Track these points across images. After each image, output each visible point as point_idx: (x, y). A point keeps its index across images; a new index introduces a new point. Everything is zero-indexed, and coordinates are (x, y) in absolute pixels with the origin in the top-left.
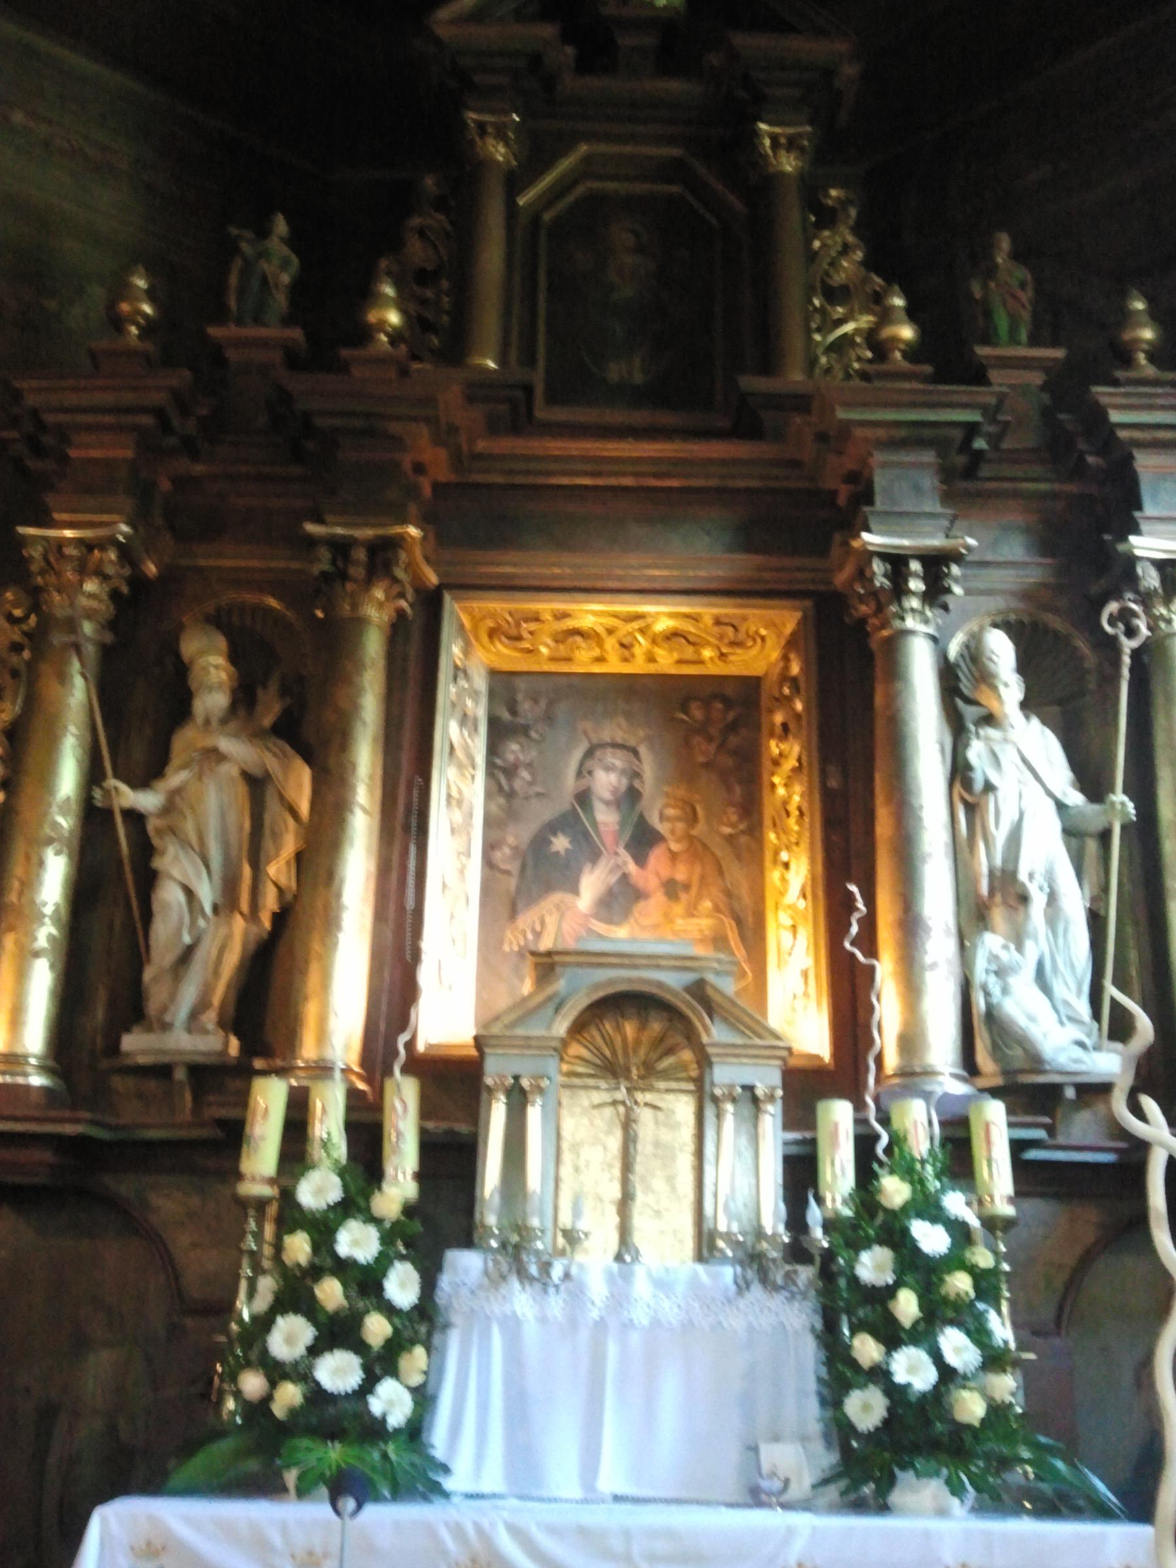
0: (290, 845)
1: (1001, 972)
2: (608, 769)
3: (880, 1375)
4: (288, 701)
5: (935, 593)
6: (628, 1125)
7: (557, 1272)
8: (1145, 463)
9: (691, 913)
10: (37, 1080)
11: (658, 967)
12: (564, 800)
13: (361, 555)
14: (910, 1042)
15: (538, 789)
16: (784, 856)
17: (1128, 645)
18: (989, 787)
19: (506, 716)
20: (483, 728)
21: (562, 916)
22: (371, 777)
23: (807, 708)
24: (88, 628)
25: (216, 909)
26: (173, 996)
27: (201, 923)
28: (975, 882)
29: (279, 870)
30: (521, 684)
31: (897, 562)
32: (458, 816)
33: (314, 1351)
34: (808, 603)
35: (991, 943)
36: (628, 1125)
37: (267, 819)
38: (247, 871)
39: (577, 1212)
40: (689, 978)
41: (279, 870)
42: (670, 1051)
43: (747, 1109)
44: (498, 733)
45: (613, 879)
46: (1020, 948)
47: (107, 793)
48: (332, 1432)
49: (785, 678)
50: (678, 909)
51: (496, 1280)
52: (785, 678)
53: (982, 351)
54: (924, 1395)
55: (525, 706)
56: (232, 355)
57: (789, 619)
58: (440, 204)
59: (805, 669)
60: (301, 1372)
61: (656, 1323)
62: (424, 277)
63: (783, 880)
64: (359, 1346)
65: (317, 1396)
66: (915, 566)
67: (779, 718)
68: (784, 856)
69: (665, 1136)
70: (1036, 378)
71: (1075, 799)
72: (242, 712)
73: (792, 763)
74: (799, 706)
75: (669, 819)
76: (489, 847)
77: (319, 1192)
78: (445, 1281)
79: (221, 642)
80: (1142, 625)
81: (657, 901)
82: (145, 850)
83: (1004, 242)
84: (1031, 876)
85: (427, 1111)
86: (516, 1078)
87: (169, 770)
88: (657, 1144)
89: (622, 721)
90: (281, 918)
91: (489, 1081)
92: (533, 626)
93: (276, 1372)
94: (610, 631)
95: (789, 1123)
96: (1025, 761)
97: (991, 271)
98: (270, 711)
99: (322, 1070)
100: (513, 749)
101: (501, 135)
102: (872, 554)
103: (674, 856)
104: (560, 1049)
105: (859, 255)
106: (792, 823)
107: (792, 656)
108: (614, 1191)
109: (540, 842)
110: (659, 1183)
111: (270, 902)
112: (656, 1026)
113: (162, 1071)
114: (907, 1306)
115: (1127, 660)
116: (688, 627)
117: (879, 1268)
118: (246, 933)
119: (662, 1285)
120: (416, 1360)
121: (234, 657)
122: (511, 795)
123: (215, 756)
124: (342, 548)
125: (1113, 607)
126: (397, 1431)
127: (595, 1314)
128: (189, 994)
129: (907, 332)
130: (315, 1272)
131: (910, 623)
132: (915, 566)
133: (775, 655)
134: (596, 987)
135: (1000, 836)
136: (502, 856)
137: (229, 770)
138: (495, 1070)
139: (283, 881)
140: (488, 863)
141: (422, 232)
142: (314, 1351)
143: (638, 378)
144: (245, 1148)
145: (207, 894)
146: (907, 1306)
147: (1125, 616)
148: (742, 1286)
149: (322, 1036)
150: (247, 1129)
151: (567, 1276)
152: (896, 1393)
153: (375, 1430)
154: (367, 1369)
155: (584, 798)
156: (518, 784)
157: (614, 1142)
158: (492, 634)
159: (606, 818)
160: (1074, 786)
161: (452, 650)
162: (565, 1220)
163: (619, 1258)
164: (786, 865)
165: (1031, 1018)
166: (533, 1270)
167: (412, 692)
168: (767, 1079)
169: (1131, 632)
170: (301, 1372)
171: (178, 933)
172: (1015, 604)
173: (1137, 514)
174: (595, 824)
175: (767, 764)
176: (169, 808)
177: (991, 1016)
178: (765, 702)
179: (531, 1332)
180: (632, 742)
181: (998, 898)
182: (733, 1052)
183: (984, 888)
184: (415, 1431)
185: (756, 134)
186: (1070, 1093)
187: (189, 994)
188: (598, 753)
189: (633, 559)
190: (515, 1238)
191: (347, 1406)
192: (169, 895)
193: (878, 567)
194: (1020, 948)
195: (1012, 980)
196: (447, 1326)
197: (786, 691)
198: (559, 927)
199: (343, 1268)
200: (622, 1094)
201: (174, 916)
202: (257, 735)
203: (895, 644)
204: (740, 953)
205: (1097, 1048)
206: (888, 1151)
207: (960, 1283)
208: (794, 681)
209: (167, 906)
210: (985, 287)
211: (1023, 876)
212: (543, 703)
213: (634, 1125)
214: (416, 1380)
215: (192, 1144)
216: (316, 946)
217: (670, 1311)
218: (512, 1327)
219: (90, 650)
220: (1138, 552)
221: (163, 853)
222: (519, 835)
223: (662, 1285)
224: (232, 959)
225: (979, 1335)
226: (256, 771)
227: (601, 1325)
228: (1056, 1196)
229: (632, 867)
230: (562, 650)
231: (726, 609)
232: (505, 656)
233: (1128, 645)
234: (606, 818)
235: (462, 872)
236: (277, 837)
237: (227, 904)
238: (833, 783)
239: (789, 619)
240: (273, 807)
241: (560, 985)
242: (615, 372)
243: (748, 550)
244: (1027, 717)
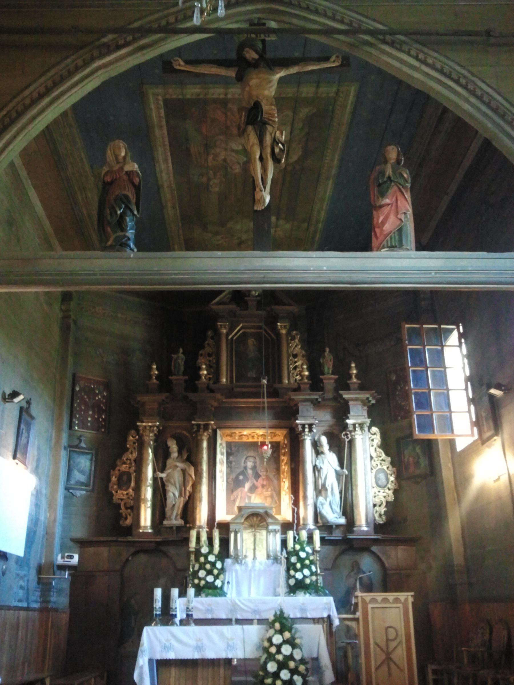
0: (191, 484)
1: (322, 504)
2: (250, 462)
3: (294, 577)
4: (188, 453)
5: (311, 430)
6: (255, 536)
7: (243, 562)
8: (351, 403)
9: (267, 491)
10: (150, 531)
11: (259, 509)
12: (242, 469)
13: (202, 427)
14: (305, 519)
15: (237, 466)
16: (284, 480)
17: (347, 440)
18: (321, 468)
19: (229, 451)
20: (225, 454)
21: (242, 492)
22: (206, 471)
23: (288, 451)
24: (152, 443)
25: (179, 497)
26: (172, 513)
27: (176, 500)
28: (318, 486)
29: (189, 488)
30: (233, 444)
31: (303, 426)
32: (221, 474)
33: (206, 575)
34: (288, 429)
35: (321, 499)
36: (255, 536)
37: (186, 478)
38: (183, 488)
39: (246, 552)
40: (264, 510)
41: (189, 488)
42: (262, 522)
43: (274, 533)
44: (229, 454)
45: (251, 485)
46: (326, 500)
47: (157, 475)
48: (209, 588)
49: (284, 444)
50: (264, 490)
51: (233, 563)
52: (284, 444)
53: (321, 377)
54: (300, 580)
55: (233, 449)
56: (174, 382)
57: (284, 432)
58: (212, 338)
59: (287, 442)
60: (204, 579)
61: (260, 570)
62: (210, 355)
63: (284, 485)
64: (213, 575)
65: (207, 582)
66: (307, 426)
67: (283, 451)
68: (284, 480)
69: (261, 537)
70: (333, 381)
71: (338, 468)
72: (180, 457)
73: (285, 461)
74: (287, 450)
75: (262, 472)
76: (227, 479)
77: (205, 550)
78: (225, 564)
79: (175, 442)
80: (349, 436)
81: (260, 489)
82: (163, 485)
83: (327, 350)
84: (328, 485)
85: (220, 534)
86: (236, 529)
87: (166, 468)
88: (260, 539)
89: (252, 451)
90: (189, 497)
91: (231, 530)
92: (234, 434)
93: (200, 579)
94: (250, 434)
95: (282, 534)
96: (328, 462)
97: (324, 357)
98: (185, 456)
99: (201, 527)
100: (231, 458)
101: (225, 328)
102: (298, 424)
103: (263, 480)
104: (243, 524)
105: (300, 346)
106: (285, 474)
107: (285, 439)
108: (253, 547)
109: (237, 477)
110: (260, 546)
111: (188, 494)
112: (259, 518)
113: (171, 528)
114: (298, 566)
115: (346, 443)
116: (266, 434)
117: (294, 560)
118: (183, 501)
119: (261, 563)
120: (222, 576)
121: (178, 444)
122: (231, 468)
123: (176, 467)
124: (198, 426)
125: (344, 433)
126: (219, 588)
127: (249, 568)
128: (175, 513)
129: (307, 373)
130: (205, 563)
131: (306, 437)
132: (307, 426)
133: (282, 438)
134: (249, 513)
135: (323, 477)
136: (230, 480)
137: (179, 469)
138: (232, 527)
139: (190, 490)
140: (227, 482)
141: (208, 344)
142: (206, 575)
143: (254, 376)
144: (190, 542)
145: (177, 494)
146: (298, 566)
147: (346, 434)
148: (273, 563)
149: (200, 521)
150: (190, 539)
151: (245, 563)
152: (296, 579)
153: (216, 588)
154: (214, 577)
155: (245, 468)
156: (232, 465)
157: (252, 539)
158: (227, 435)
159: (250, 472)
160: (339, 466)
161: (219, 441)
162: (244, 554)
163: (253, 559)
164: (284, 482)
165: (327, 513)
166: (239, 562)
167: (212, 453)
168: (278, 528)
169: (348, 438)
170: (204, 579)
171: (172, 502)
172: (328, 428)
173: (349, 415)
174: (248, 474)
175: (281, 461)
176: (167, 476)
177: (320, 512)
178: (281, 448)
179: (239, 572)
180: (255, 456)
181: (323, 489)
182: (272, 524)
183: (320, 488)
184: (222, 588)
185: (277, 325)
186: (334, 527)
187: (175, 513)
188: (248, 458)
189: (255, 421)
190: (236, 557)
191: (212, 584)
192: (170, 495)
193: (300, 426)
194: (326, 500)
195: (324, 506)
196: (226, 571)
197: (284, 446)
198: (241, 495)
199: (210, 562)
200: (253, 530)
201: (171, 499)
202: (183, 461)
203: (303, 441)
204: (276, 499)
205: (340, 518)
206: (298, 540)
207: (307, 562)
208: (286, 445)
209: (170, 497)
210: (323, 360)
211: (327, 486)
212: (237, 448)
213: (274, 474)
214: (222, 580)
215: (177, 541)
216: (198, 504)
217: (262, 568)
218: (236, 571)
219: (152, 447)
220: (348, 423)
221: (168, 486)
222: (233, 476)
223: (261, 563)
224: (181, 505)
225: (310, 570)
226: (184, 469)
227: (251, 570)
228: (332, 545)
229: (255, 482)
230: (240, 438)
231: (272, 430)
232: (229, 439)
233: (347, 440)
234: (250, 472)
235: (222, 485)
236: (189, 483)
237: (180, 495)
238: (293, 466)
239: (284, 432)
240: (187, 477)
241: (242, 513)
242: (249, 375)
243: (276, 419)
244: (330, 452)
